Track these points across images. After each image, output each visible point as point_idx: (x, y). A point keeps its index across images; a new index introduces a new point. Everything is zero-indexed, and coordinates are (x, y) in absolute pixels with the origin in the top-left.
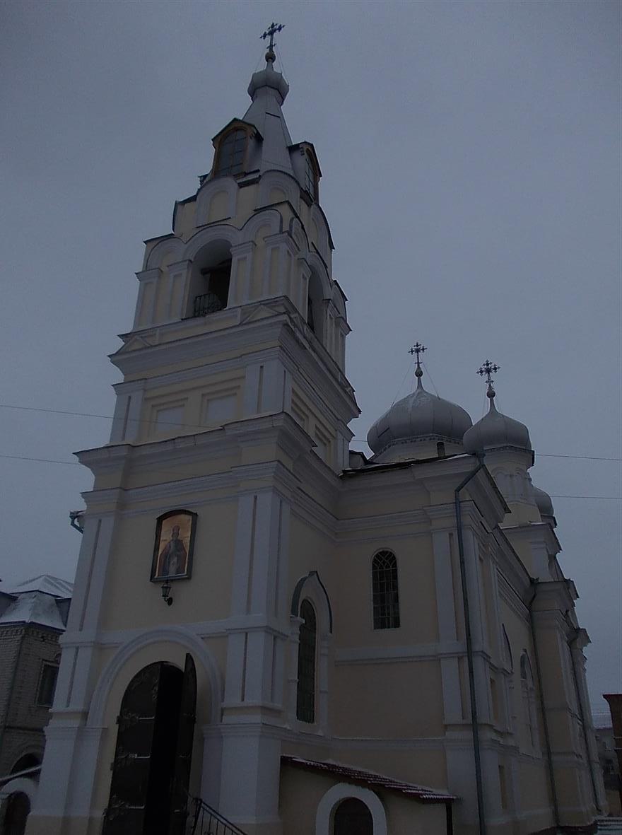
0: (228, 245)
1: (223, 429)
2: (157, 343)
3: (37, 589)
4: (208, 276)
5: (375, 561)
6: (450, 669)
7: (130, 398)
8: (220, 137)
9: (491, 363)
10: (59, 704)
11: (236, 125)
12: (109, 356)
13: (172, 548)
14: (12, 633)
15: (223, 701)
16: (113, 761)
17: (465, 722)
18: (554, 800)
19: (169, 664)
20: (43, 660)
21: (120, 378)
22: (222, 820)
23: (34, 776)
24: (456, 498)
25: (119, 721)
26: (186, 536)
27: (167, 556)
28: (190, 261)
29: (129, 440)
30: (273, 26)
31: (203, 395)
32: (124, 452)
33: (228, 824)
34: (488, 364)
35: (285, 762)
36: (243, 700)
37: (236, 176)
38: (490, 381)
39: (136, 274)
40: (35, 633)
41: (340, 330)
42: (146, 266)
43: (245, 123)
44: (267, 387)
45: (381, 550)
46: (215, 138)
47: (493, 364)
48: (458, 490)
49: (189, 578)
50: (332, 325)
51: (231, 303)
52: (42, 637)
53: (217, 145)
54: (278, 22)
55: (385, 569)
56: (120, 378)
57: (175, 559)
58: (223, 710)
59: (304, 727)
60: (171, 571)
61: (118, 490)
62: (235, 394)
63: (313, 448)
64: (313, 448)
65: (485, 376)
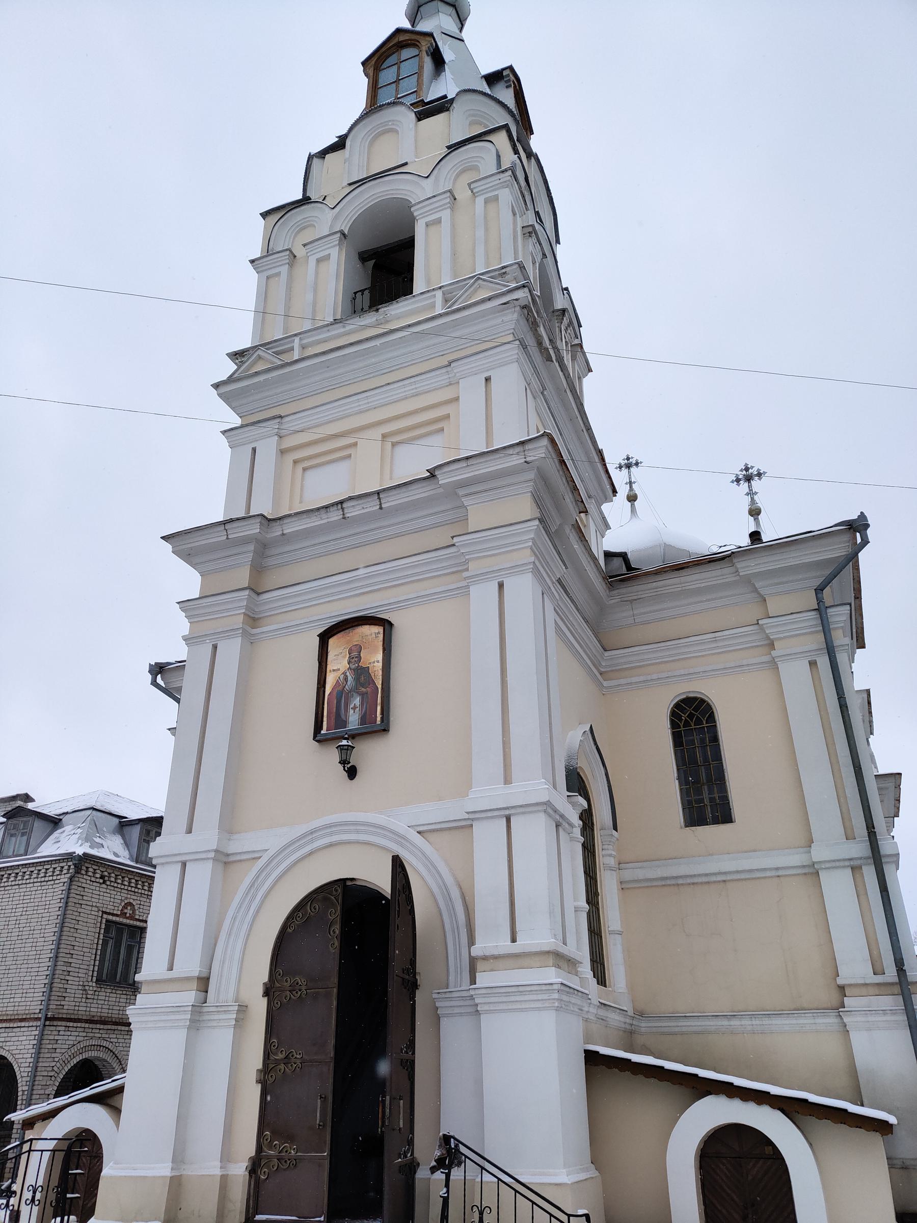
1: (432, 474)
2: (296, 357)
3: (89, 805)
6: (839, 889)
7: (254, 450)
9: (752, 467)
10: (152, 964)
11: (402, 38)
12: (216, 386)
13: (349, 683)
14: (54, 872)
15: (471, 942)
16: (260, 1066)
17: (879, 979)
19: (358, 883)
20: (103, 912)
21: (235, 420)
23: (110, 1100)
24: (820, 601)
25: (269, 991)
26: (374, 660)
27: (342, 695)
28: (344, 234)
29: (263, 505)
31: (384, 436)
32: (254, 529)
35: (591, 1058)
36: (514, 940)
38: (751, 493)
39: (252, 262)
40: (91, 870)
42: (268, 252)
44: (496, 408)
45: (684, 696)
49: (385, 730)
51: (419, 285)
52: (102, 877)
53: (371, 72)
55: (693, 722)
56: (235, 420)
57: (357, 701)
58: (473, 963)
60: (351, 720)
61: (247, 592)
65: (744, 486)
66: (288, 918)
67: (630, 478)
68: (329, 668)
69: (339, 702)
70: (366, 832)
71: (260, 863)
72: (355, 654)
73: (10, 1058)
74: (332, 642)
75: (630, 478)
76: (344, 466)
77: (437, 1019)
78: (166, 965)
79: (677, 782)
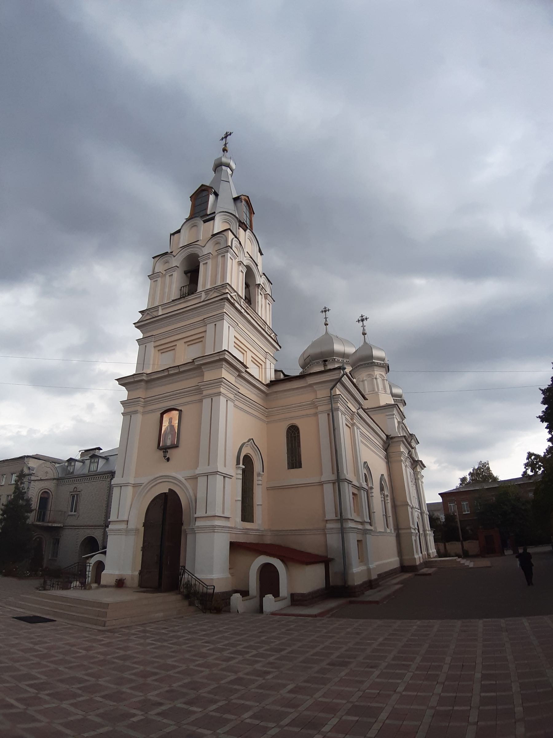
1: (193, 361)
4: (189, 274)
5: (288, 431)
6: (328, 489)
8: (194, 196)
11: (203, 188)
12: (134, 324)
17: (336, 518)
18: (400, 553)
21: (141, 336)
25: (145, 525)
26: (176, 423)
30: (227, 133)
34: (362, 317)
37: (202, 217)
38: (363, 326)
41: (267, 301)
48: (332, 389)
51: (200, 288)
53: (193, 200)
54: (229, 131)
56: (141, 336)
57: (170, 436)
59: (248, 525)
62: (202, 341)
63: (247, 370)
64: (247, 370)
65: (361, 323)
68: (163, 425)
71: (142, 487)
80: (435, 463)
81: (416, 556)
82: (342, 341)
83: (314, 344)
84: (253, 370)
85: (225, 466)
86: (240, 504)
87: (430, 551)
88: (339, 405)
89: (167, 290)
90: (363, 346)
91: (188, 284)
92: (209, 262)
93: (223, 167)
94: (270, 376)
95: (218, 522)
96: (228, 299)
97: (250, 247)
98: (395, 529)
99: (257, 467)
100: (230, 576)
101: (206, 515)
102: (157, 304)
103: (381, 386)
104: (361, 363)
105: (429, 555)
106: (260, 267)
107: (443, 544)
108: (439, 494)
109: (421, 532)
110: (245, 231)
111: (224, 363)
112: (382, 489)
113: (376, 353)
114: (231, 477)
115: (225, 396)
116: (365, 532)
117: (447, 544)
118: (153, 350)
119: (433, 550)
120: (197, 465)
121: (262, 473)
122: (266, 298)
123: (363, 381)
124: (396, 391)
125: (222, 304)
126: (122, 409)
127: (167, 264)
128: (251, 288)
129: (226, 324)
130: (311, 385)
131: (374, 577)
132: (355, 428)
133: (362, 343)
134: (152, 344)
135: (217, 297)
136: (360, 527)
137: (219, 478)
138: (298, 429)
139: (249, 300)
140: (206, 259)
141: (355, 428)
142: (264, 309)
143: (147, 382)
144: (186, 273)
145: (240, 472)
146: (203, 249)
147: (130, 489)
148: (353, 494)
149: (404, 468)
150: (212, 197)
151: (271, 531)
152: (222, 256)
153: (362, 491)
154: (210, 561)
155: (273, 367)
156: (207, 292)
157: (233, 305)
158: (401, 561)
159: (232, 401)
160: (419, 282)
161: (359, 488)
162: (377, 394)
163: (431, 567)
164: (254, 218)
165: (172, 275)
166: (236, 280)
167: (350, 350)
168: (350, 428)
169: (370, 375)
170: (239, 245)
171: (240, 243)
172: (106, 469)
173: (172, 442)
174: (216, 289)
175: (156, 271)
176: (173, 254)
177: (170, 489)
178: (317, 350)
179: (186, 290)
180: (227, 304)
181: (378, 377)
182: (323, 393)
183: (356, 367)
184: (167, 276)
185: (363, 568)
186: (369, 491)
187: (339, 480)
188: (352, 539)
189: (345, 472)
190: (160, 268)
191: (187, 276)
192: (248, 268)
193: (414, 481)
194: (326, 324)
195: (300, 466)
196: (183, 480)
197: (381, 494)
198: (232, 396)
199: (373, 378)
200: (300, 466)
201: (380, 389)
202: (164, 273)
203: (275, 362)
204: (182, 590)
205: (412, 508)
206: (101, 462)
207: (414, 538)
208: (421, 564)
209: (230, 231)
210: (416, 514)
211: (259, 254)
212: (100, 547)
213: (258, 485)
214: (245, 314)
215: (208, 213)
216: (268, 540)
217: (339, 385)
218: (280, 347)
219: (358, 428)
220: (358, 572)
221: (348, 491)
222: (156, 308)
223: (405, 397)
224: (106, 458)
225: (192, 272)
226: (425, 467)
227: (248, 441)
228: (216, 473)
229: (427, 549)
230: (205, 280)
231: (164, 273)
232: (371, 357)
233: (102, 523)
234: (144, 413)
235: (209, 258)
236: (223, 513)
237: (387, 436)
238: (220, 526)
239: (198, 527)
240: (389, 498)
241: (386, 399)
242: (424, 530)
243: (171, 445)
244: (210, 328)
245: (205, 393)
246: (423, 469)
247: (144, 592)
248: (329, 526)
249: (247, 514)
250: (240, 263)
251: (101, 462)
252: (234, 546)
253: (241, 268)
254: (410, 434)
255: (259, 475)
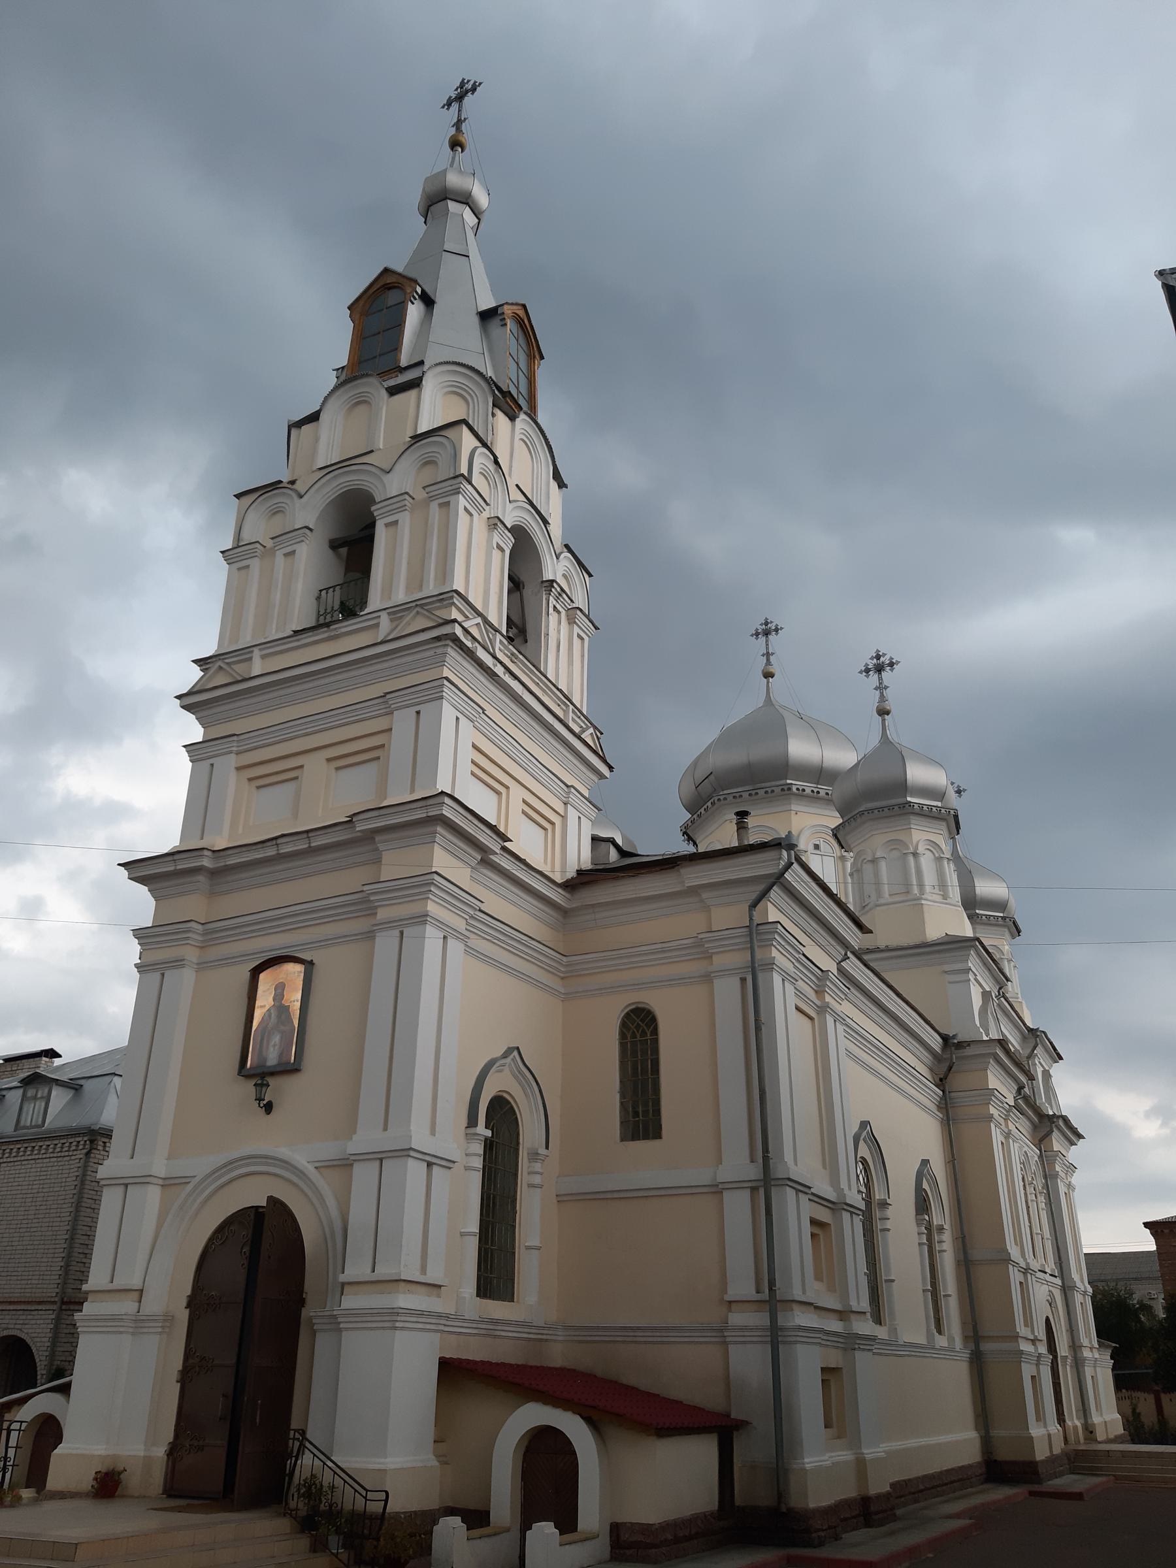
0: (369, 499)
1: (350, 822)
4: (344, 551)
5: (624, 1025)
6: (738, 1206)
8: (361, 303)
9: (884, 655)
11: (389, 279)
18: (983, 1416)
21: (196, 733)
22: (330, 1464)
23: (65, 1390)
26: (294, 998)
33: (338, 1471)
37: (384, 374)
38: (881, 688)
41: (576, 630)
43: (404, 277)
46: (352, 304)
47: (887, 657)
48: (754, 905)
50: (560, 622)
51: (375, 600)
54: (473, 78)
56: (196, 733)
57: (276, 1039)
59: (497, 1309)
63: (507, 844)
64: (507, 844)
66: (211, 1240)
67: (767, 648)
68: (258, 1003)
69: (262, 1039)
70: (275, 1165)
71: (189, 1187)
72: (279, 991)
73: (28, 1341)
74: (262, 976)
75: (767, 648)
76: (291, 786)
77: (314, 1333)
78: (109, 1279)
79: (618, 1096)
80: (1148, 1115)
81: (1036, 1431)
82: (814, 728)
83: (727, 738)
84: (527, 841)
85: (433, 1133)
86: (473, 1244)
87: (1096, 1419)
88: (775, 953)
89: (277, 596)
90: (876, 751)
91: (336, 568)
92: (405, 519)
93: (452, 206)
94: (579, 855)
95: (405, 1300)
96: (456, 640)
97: (524, 466)
98: (966, 1338)
99: (530, 1132)
100: (434, 1463)
101: (374, 1277)
102: (246, 640)
103: (930, 878)
104: (870, 805)
105: (1089, 1430)
106: (556, 529)
107: (1151, 1398)
108: (1147, 1225)
109: (1063, 1349)
110: (512, 418)
111: (439, 829)
112: (922, 1205)
113: (918, 773)
114: (447, 1164)
115: (440, 924)
116: (851, 1343)
117: (1165, 1398)
118: (233, 776)
119: (1108, 1416)
120: (351, 1126)
121: (542, 1151)
122: (571, 621)
123: (874, 861)
124: (986, 888)
125: (439, 651)
126: (133, 949)
127: (279, 516)
128: (527, 592)
129: (448, 713)
130: (694, 891)
131: (878, 1486)
132: (830, 1020)
133: (874, 740)
134: (232, 761)
135: (423, 630)
136: (835, 1325)
137: (415, 1170)
138: (653, 1020)
139: (520, 631)
140: (391, 512)
141: (830, 1020)
142: (565, 655)
143: (214, 873)
144: (334, 545)
145: (478, 1148)
146: (386, 478)
147: (153, 1194)
148: (814, 1222)
149: (997, 1137)
150: (414, 311)
151: (567, 1328)
152: (441, 505)
153: (846, 1216)
154: (378, 1417)
155: (587, 831)
156: (397, 612)
157: (470, 654)
158: (987, 1442)
159: (462, 938)
160: (1075, 536)
161: (837, 1206)
162: (917, 905)
163: (1092, 1472)
164: (542, 372)
165: (294, 552)
166: (480, 576)
167: (843, 757)
168: (811, 1018)
169: (897, 845)
170: (492, 467)
171: (496, 462)
172: (75, 1121)
173: (281, 1055)
174: (422, 606)
175: (247, 537)
176: (297, 486)
177: (271, 1199)
178: (736, 757)
179: (334, 599)
180: (452, 653)
181: (921, 849)
182: (728, 915)
183: (854, 818)
184: (279, 555)
185: (844, 1456)
186: (871, 1214)
187: (767, 1182)
188: (806, 1365)
189: (788, 1157)
190: (258, 528)
191: (338, 556)
192: (520, 534)
193: (1039, 1182)
194: (768, 675)
195: (658, 1135)
196: (310, 1169)
197: (919, 1225)
198: (461, 925)
199: (905, 853)
200: (658, 1135)
201: (928, 889)
202: (269, 544)
203: (593, 813)
204: (292, 1504)
205: (1026, 1271)
206: (59, 1098)
207: (1027, 1370)
208: (1052, 1460)
209: (465, 429)
210: (1043, 1292)
211: (554, 485)
212: (41, 1370)
213: (531, 1186)
214: (507, 679)
215: (404, 361)
216: (557, 1356)
217: (776, 893)
218: (611, 768)
219: (839, 1018)
220: (822, 1467)
221: (795, 1215)
222: (244, 654)
223: (1018, 911)
224: (74, 1086)
225: (354, 543)
226: (1080, 1136)
227: (505, 1055)
228: (406, 1152)
229: (1085, 1411)
230: (391, 578)
231: (269, 544)
232: (902, 786)
233: (49, 1288)
234: (202, 967)
235: (402, 509)
236: (423, 1270)
237: (945, 1039)
238: (411, 1312)
239: (353, 1313)
240: (947, 1236)
241: (946, 919)
242: (1075, 1347)
243: (279, 1064)
244: (402, 722)
245: (382, 914)
246: (1072, 1144)
247: (180, 1509)
248: (737, 1318)
249: (495, 1274)
250: (495, 523)
251: (59, 1098)
252: (452, 1372)
253: (496, 538)
254: (1030, 1030)
255: (534, 1156)
